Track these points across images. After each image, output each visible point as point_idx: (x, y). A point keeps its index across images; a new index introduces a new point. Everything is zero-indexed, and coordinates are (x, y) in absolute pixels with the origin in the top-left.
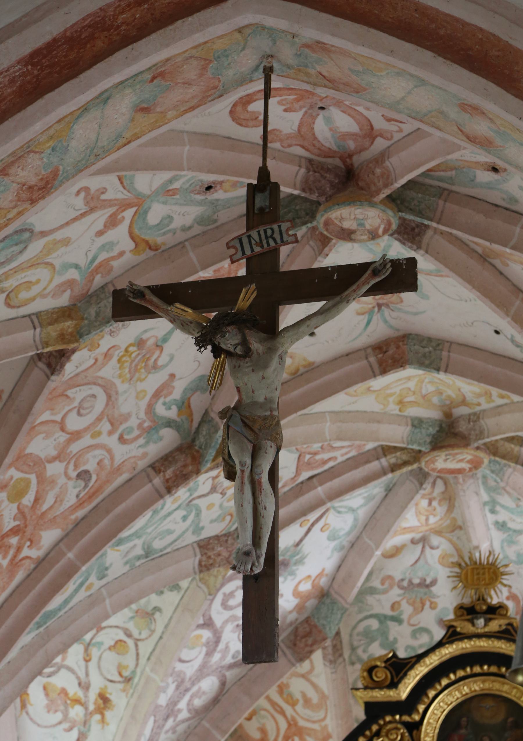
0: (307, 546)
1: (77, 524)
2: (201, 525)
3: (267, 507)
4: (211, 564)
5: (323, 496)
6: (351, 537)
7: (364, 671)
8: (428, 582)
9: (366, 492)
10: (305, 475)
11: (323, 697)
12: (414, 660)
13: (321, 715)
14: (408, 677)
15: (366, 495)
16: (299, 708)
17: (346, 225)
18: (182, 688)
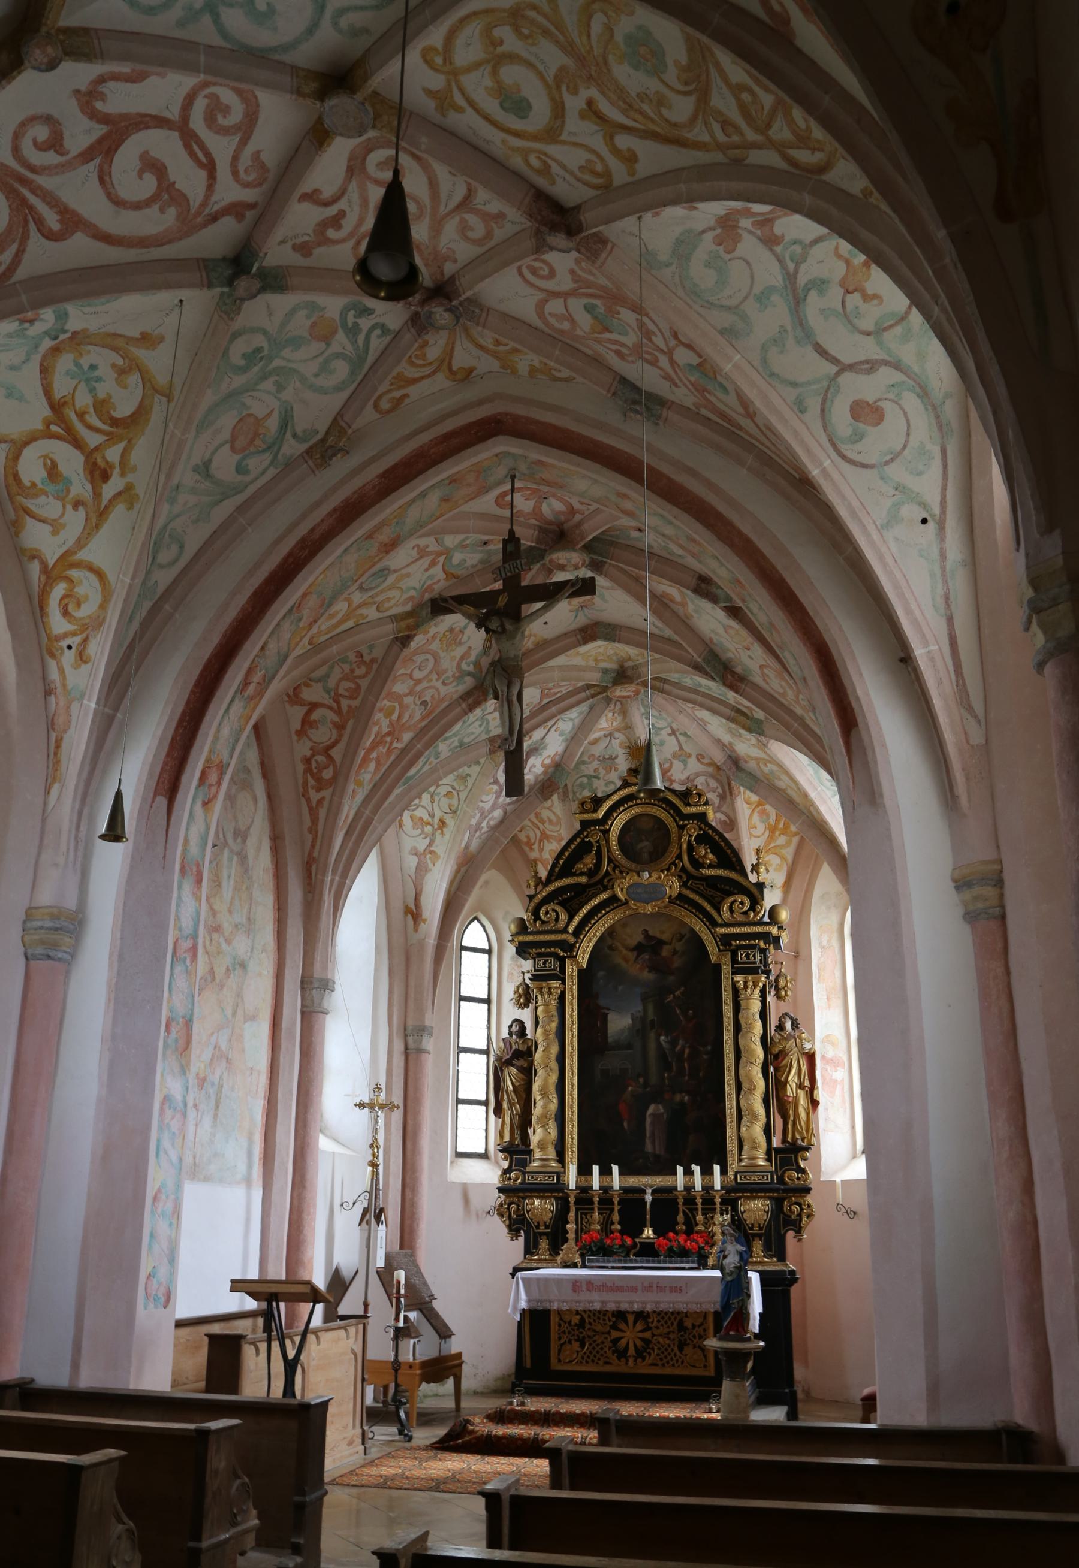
0: (548, 739)
1: (422, 729)
10: (545, 701)
17: (561, 562)
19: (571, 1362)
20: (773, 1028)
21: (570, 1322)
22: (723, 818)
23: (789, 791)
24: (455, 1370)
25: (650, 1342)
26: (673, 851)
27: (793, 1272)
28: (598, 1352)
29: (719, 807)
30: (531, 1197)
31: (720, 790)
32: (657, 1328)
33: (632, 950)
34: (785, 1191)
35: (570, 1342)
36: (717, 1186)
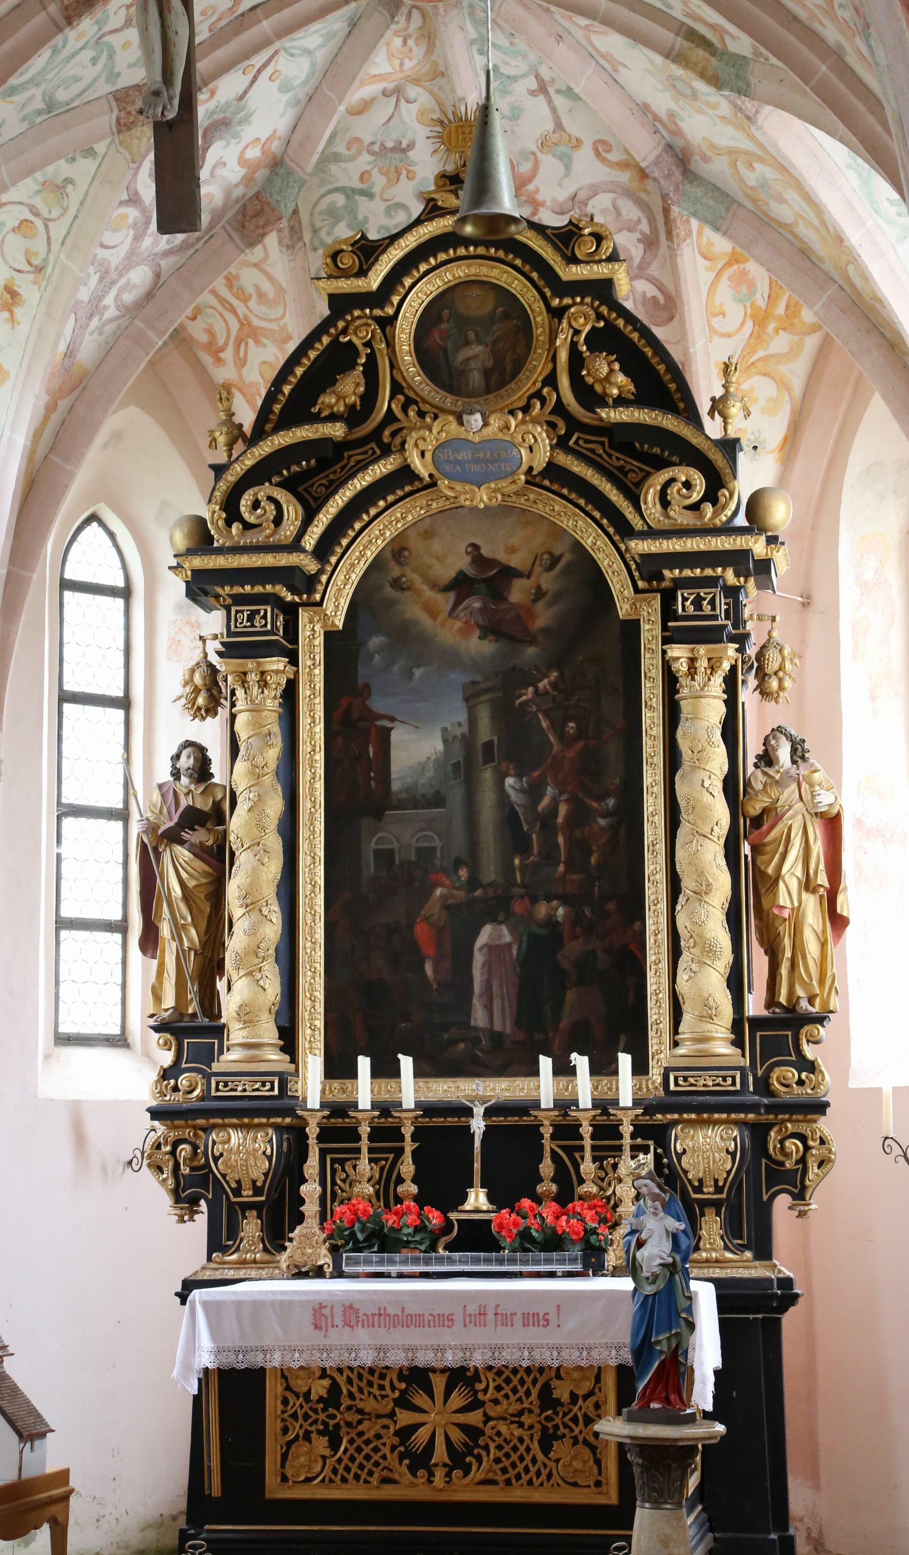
2: (116, 70)
3: (179, 32)
4: (133, 122)
5: (270, 33)
6: (308, 89)
7: (327, 256)
8: (404, 145)
9: (325, 27)
11: (280, 290)
12: (387, 242)
13: (279, 311)
14: (380, 262)
15: (324, 31)
16: (252, 304)
18: (107, 280)
19: (308, 1480)
20: (751, 760)
21: (307, 1395)
22: (652, 291)
23: (802, 230)
24: (54, 1509)
25: (483, 1433)
26: (538, 367)
27: (786, 1283)
28: (368, 1457)
29: (640, 267)
30: (224, 1127)
31: (645, 227)
32: (496, 1402)
33: (446, 589)
34: (770, 1109)
35: (307, 1437)
36: (626, 1099)
